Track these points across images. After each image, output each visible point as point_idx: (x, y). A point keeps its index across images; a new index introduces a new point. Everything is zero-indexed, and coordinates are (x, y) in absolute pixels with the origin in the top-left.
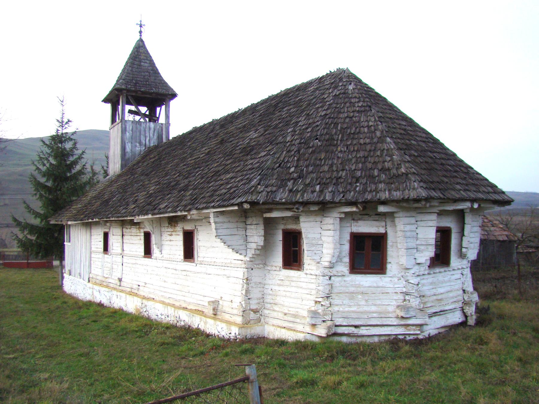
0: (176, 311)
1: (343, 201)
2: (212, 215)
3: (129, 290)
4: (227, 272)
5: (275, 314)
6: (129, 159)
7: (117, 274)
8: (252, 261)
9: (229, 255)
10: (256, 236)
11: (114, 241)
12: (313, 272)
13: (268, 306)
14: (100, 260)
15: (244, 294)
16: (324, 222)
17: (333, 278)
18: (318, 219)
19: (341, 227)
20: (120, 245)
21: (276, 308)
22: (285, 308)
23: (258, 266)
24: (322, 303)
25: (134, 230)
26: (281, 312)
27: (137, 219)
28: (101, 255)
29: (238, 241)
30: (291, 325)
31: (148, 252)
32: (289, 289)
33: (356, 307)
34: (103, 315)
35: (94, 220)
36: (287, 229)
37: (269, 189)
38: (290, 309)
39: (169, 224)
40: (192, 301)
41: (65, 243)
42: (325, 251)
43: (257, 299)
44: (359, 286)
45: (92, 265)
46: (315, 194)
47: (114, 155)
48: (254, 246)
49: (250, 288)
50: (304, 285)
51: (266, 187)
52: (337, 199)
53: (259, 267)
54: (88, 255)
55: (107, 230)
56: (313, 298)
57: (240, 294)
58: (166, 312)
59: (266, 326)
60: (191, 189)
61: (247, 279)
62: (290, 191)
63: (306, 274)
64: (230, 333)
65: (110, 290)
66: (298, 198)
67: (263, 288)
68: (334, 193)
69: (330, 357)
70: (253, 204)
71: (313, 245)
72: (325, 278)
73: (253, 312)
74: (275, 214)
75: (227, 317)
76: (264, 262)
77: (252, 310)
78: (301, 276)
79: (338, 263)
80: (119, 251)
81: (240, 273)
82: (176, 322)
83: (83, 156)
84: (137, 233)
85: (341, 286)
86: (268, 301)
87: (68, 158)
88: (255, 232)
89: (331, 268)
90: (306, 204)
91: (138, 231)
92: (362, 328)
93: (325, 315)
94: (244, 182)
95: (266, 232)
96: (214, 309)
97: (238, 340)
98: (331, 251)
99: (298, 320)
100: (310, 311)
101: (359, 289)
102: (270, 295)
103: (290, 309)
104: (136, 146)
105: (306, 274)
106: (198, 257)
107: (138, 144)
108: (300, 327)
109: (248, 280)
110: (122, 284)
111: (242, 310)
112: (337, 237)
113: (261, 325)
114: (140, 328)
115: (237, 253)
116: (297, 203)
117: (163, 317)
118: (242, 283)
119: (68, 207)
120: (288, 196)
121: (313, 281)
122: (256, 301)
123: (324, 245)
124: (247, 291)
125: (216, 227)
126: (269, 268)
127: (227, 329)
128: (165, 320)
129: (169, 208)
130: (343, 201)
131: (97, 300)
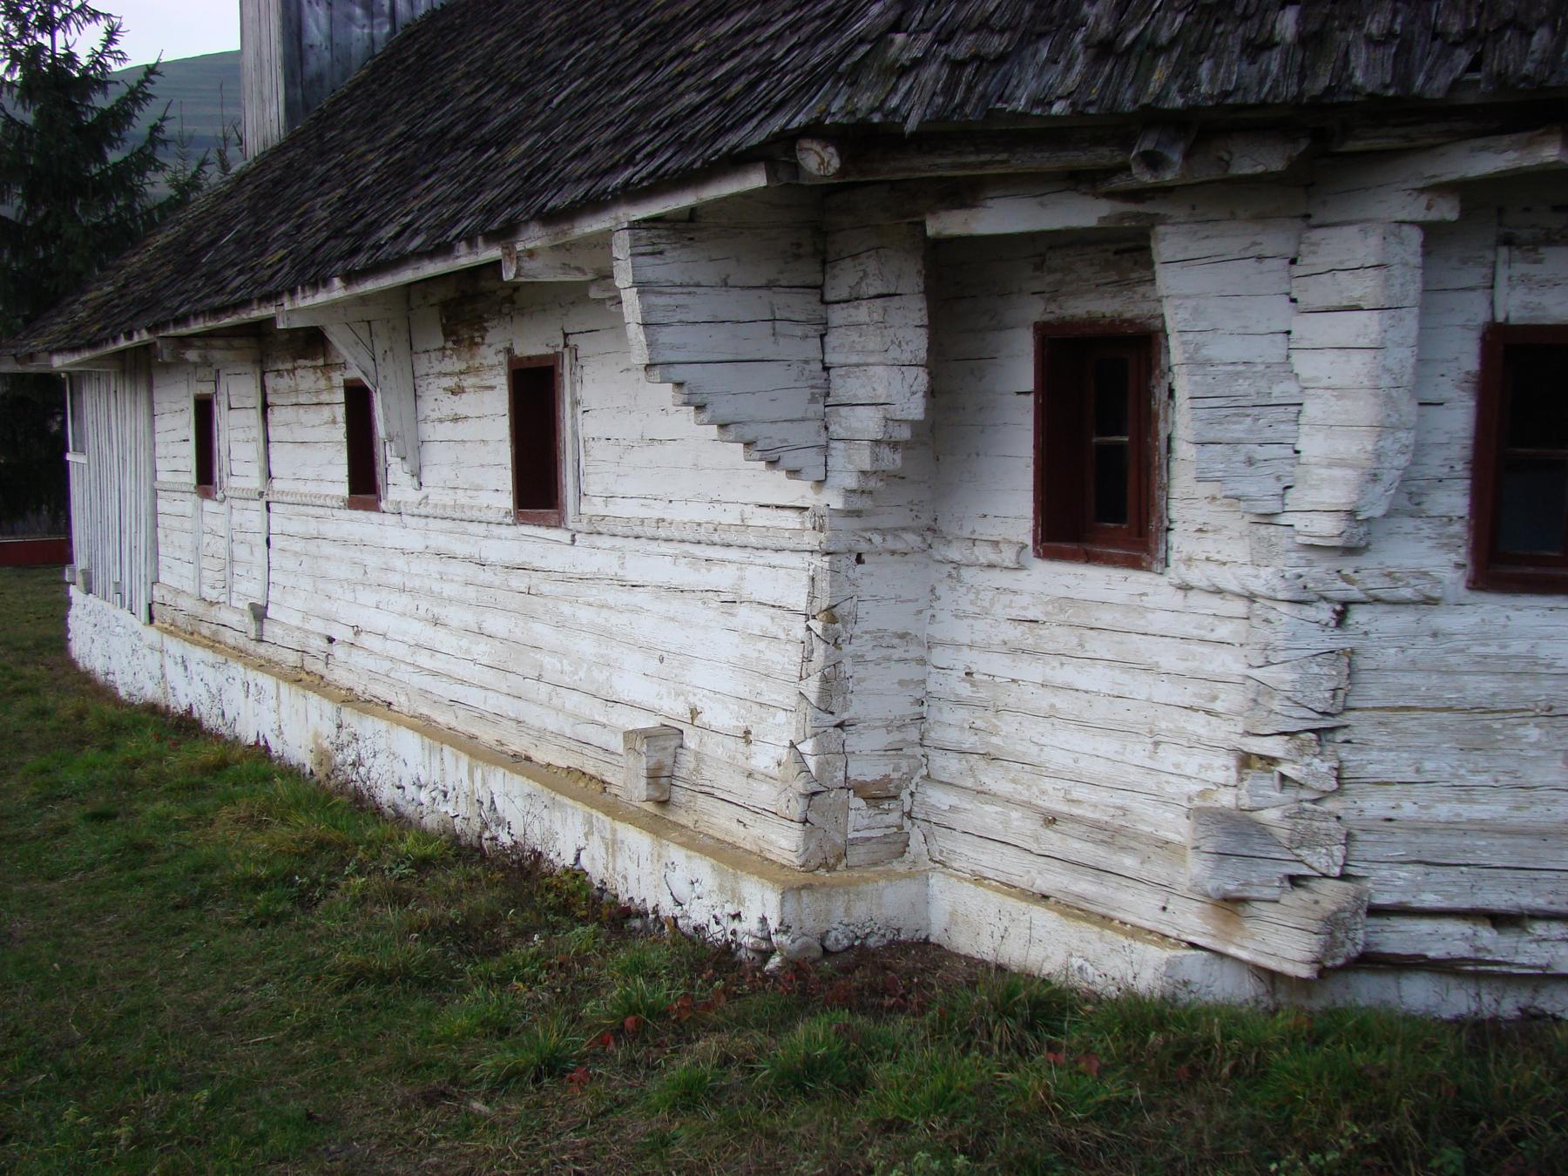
0: (478, 775)
1: (1481, 90)
2: (621, 247)
3: (292, 659)
4: (721, 577)
5: (988, 816)
6: (320, 77)
7: (249, 589)
8: (857, 513)
9: (745, 489)
10: (881, 367)
11: (236, 434)
12: (1227, 579)
13: (948, 765)
14: (188, 525)
15: (813, 697)
16: (1308, 262)
17: (1358, 616)
18: (1275, 241)
19: (1429, 290)
20: (253, 451)
21: (992, 779)
22: (1048, 784)
23: (891, 543)
24: (1286, 769)
25: (307, 379)
26: (1026, 805)
27: (298, 309)
28: (189, 503)
29: (776, 395)
30: (1084, 886)
31: (364, 483)
32: (1067, 674)
33: (1506, 797)
34: (158, 779)
35: (136, 338)
36: (1064, 324)
37: (962, 48)
38: (1079, 792)
39: (448, 333)
40: (559, 723)
41: (69, 457)
42: (1313, 445)
43: (889, 727)
44: (1531, 667)
45: (162, 550)
46: (1273, 62)
47: (260, 66)
48: (867, 423)
49: (847, 668)
50: (1168, 657)
51: (945, 38)
52: (1432, 82)
53: (899, 546)
54: (145, 504)
55: (206, 389)
56: (1228, 732)
57: (793, 700)
58: (436, 777)
59: (937, 881)
60: (531, 132)
61: (831, 615)
62: (1104, 49)
63: (1186, 588)
64: (737, 916)
65: (221, 659)
66: (1154, 86)
67: (922, 662)
68: (1405, 48)
69: (1374, 1149)
70: (859, 140)
71: (1239, 407)
72: (1310, 612)
73: (866, 799)
74: (998, 218)
75: (722, 821)
76: (925, 520)
77: (860, 789)
78: (1148, 601)
79: (1393, 523)
80: (255, 482)
81: (789, 581)
82: (476, 825)
83: (150, 89)
84: (318, 392)
85: (1413, 667)
86: (951, 736)
87: (85, 96)
88: (873, 342)
89: (1349, 551)
90: (1207, 127)
91: (322, 383)
92: (1539, 928)
93: (1307, 840)
94: (807, 30)
95: (935, 348)
96: (654, 776)
97: (774, 962)
98: (1357, 446)
99: (1129, 863)
100: (1207, 817)
101: (1527, 688)
102: (959, 702)
103: (1079, 792)
104: (350, 18)
105: (1186, 588)
106: (581, 495)
107: (358, 11)
108: (1141, 907)
109: (833, 620)
110: (271, 631)
111: (800, 786)
112: (1402, 357)
113: (909, 875)
114: (280, 865)
115: (773, 464)
116: (1152, 117)
117: (424, 796)
118: (800, 632)
119: (71, 299)
120: (1086, 81)
121: (1224, 631)
122: (881, 739)
123: (1312, 409)
124: (832, 684)
125: (646, 311)
126: (954, 553)
127: (721, 889)
128: (436, 812)
129: (416, 233)
130: (1469, 98)
131: (179, 703)
